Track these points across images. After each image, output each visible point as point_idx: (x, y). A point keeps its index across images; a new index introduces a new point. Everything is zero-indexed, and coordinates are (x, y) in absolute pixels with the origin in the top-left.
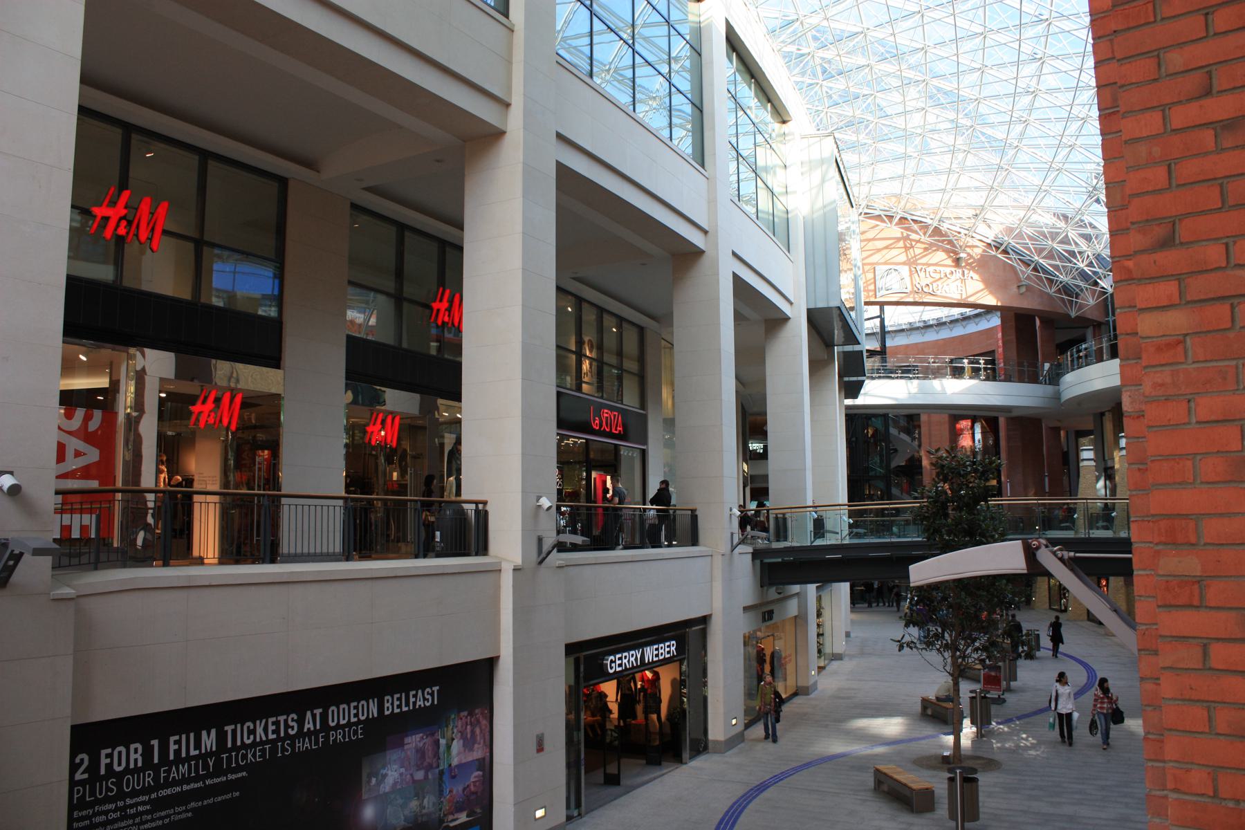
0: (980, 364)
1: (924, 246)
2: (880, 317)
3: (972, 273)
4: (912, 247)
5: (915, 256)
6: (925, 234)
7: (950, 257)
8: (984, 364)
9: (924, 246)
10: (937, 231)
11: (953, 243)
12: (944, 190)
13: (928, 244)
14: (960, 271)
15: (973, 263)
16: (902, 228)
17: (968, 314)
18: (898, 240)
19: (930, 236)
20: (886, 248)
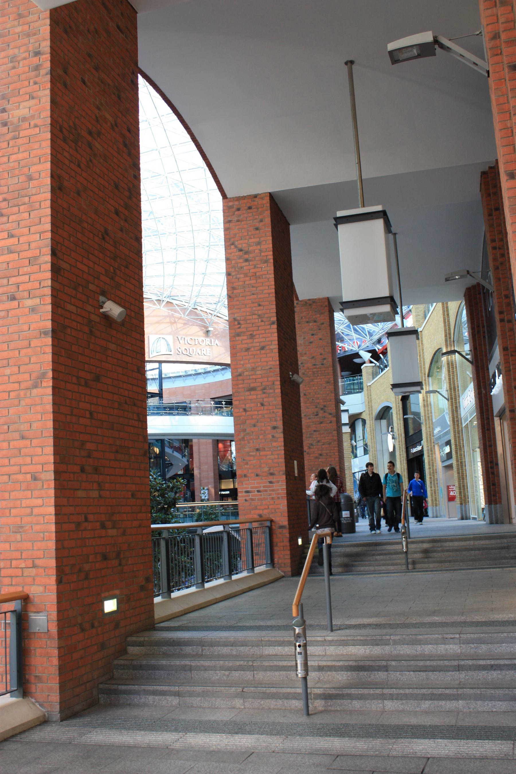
0: (222, 404)
1: (183, 322)
2: (159, 368)
3: (217, 342)
4: (175, 322)
5: (177, 329)
6: (184, 314)
7: (202, 330)
8: (225, 404)
9: (183, 322)
10: (193, 312)
11: (204, 321)
12: (202, 285)
13: (186, 320)
14: (209, 340)
15: (217, 334)
16: (168, 309)
17: (209, 370)
18: (166, 317)
19: (188, 315)
20: (157, 322)
